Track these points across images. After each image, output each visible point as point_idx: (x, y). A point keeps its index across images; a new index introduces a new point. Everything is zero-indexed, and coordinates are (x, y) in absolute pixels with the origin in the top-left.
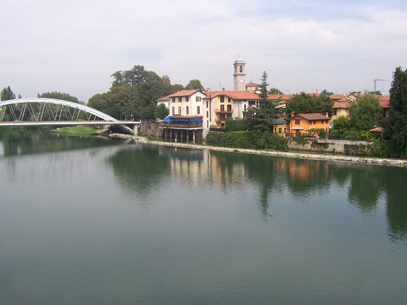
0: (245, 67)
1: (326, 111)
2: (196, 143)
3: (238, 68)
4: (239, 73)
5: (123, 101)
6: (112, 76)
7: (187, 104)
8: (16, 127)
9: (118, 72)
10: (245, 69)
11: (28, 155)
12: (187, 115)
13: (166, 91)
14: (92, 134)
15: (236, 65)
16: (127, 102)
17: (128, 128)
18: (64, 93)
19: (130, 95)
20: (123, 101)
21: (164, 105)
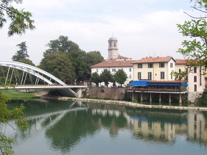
0: (117, 43)
1: (119, 81)
2: (183, 105)
3: (113, 44)
4: (113, 48)
5: (60, 67)
6: (17, 46)
7: (162, 70)
8: (54, 89)
9: (23, 43)
10: (118, 45)
11: (203, 116)
12: (162, 80)
13: (91, 59)
14: (33, 98)
15: (110, 41)
16: (64, 68)
17: (73, 92)
18: (102, 56)
19: (66, 62)
20: (60, 67)
21: (109, 72)
